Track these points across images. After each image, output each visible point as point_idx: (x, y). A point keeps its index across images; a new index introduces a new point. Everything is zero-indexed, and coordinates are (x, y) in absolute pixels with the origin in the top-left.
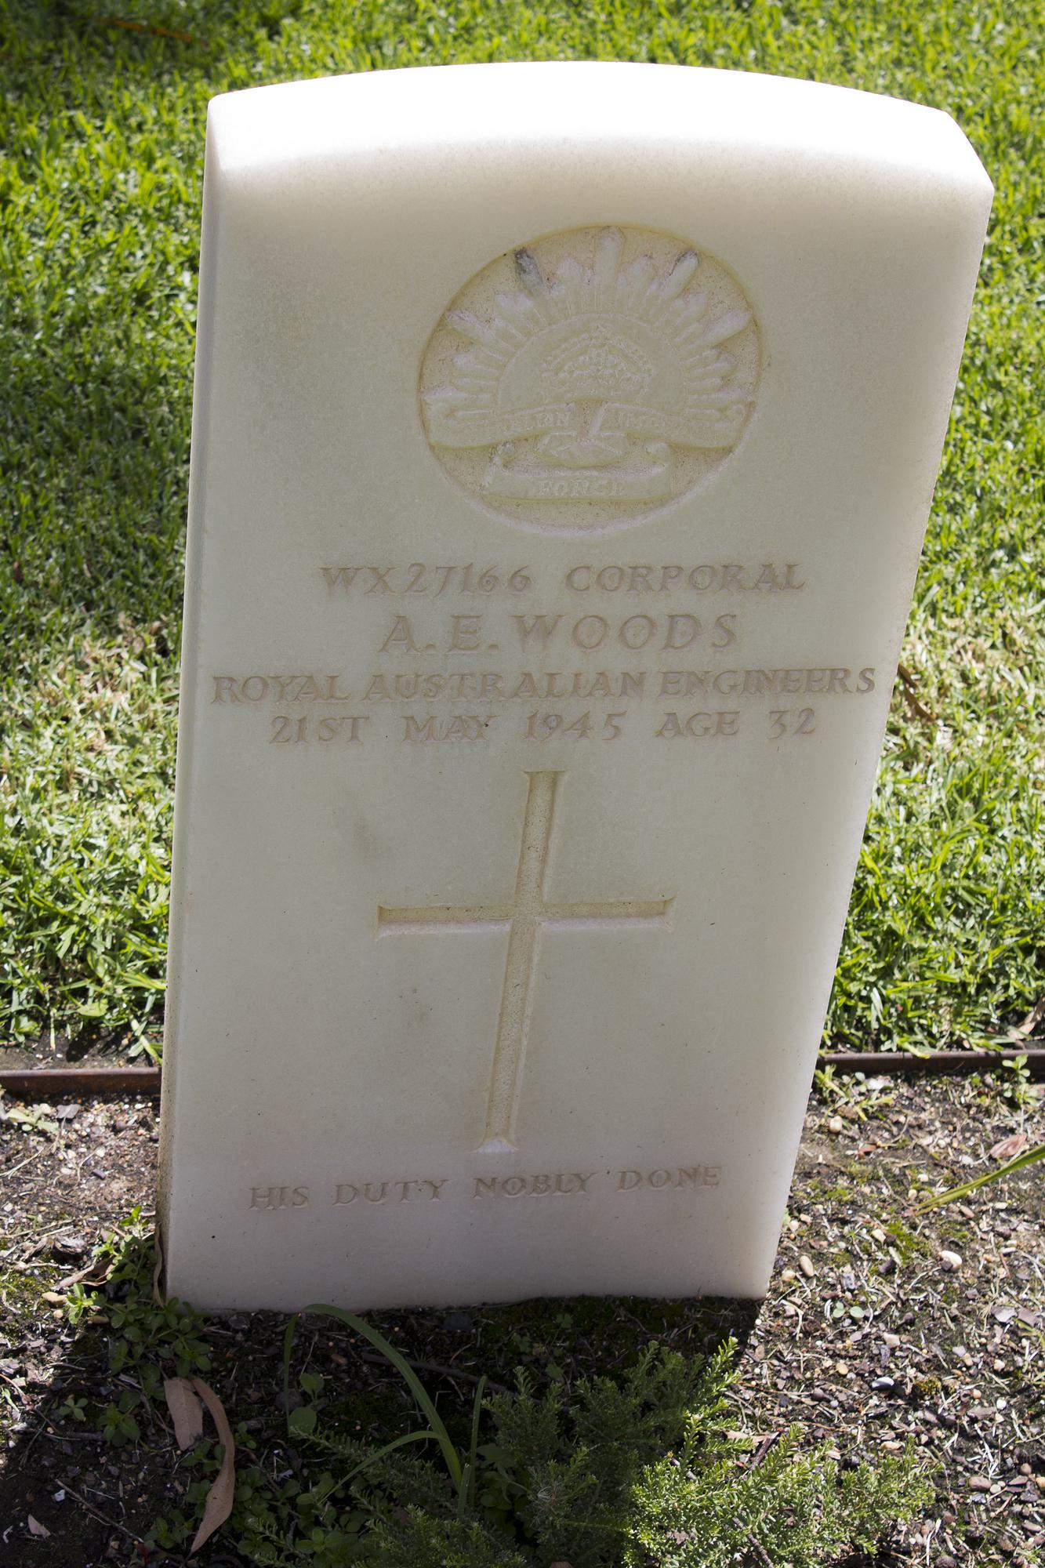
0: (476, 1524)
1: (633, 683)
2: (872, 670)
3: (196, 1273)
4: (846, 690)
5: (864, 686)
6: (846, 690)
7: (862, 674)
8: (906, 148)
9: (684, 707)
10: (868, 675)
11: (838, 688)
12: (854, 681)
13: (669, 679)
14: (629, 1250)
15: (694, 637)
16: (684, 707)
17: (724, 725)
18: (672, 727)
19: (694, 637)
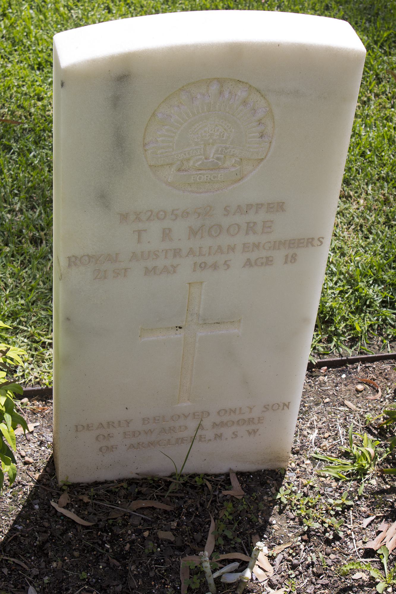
0: (37, 507)
1: (232, 249)
2: (323, 238)
3: (65, 473)
4: (313, 245)
5: (319, 244)
6: (313, 245)
7: (319, 239)
8: (338, 35)
9: (253, 256)
10: (321, 239)
11: (310, 245)
12: (316, 242)
13: (245, 247)
14: (222, 454)
15: (220, 233)
16: (253, 256)
17: (269, 261)
18: (249, 263)
19: (220, 233)
